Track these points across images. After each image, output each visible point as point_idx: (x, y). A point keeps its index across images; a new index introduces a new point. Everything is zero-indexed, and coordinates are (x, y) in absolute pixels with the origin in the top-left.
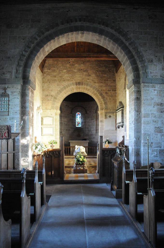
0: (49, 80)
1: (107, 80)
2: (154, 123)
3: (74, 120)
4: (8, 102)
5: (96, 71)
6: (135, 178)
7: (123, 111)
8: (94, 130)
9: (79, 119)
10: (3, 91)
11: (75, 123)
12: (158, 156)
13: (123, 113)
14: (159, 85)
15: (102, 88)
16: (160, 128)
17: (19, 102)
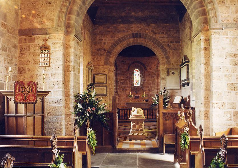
0: (101, 32)
1: (170, 31)
2: (227, 78)
3: (130, 78)
4: (48, 55)
5: (157, 20)
6: (202, 148)
7: (188, 65)
8: (155, 89)
9: (137, 76)
10: (44, 43)
11: (133, 81)
12: (232, 120)
13: (188, 69)
14: (232, 31)
15: (163, 39)
16: (234, 84)
17: (62, 55)
